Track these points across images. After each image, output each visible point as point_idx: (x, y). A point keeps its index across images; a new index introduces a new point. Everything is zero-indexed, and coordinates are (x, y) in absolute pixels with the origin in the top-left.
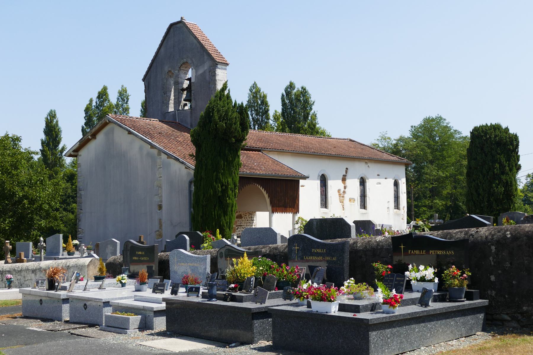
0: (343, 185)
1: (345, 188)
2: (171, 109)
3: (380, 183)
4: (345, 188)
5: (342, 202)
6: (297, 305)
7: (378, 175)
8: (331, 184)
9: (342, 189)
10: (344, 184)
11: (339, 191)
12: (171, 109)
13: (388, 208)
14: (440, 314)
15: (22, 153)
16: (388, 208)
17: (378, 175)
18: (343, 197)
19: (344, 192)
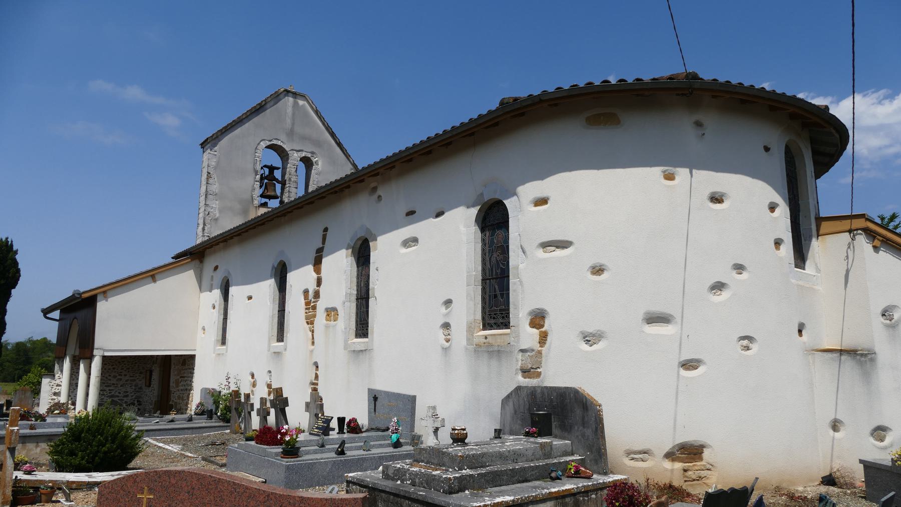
0: (315, 276)
1: (319, 282)
2: (372, 443)
3: (415, 240)
4: (319, 282)
5: (312, 323)
6: (208, 436)
7: (411, 213)
8: (293, 277)
9: (312, 287)
10: (318, 270)
11: (306, 292)
12: (372, 443)
13: (446, 326)
14: (211, 247)
15: (125, 410)
16: (446, 326)
17: (411, 213)
18: (314, 308)
19: (317, 295)
